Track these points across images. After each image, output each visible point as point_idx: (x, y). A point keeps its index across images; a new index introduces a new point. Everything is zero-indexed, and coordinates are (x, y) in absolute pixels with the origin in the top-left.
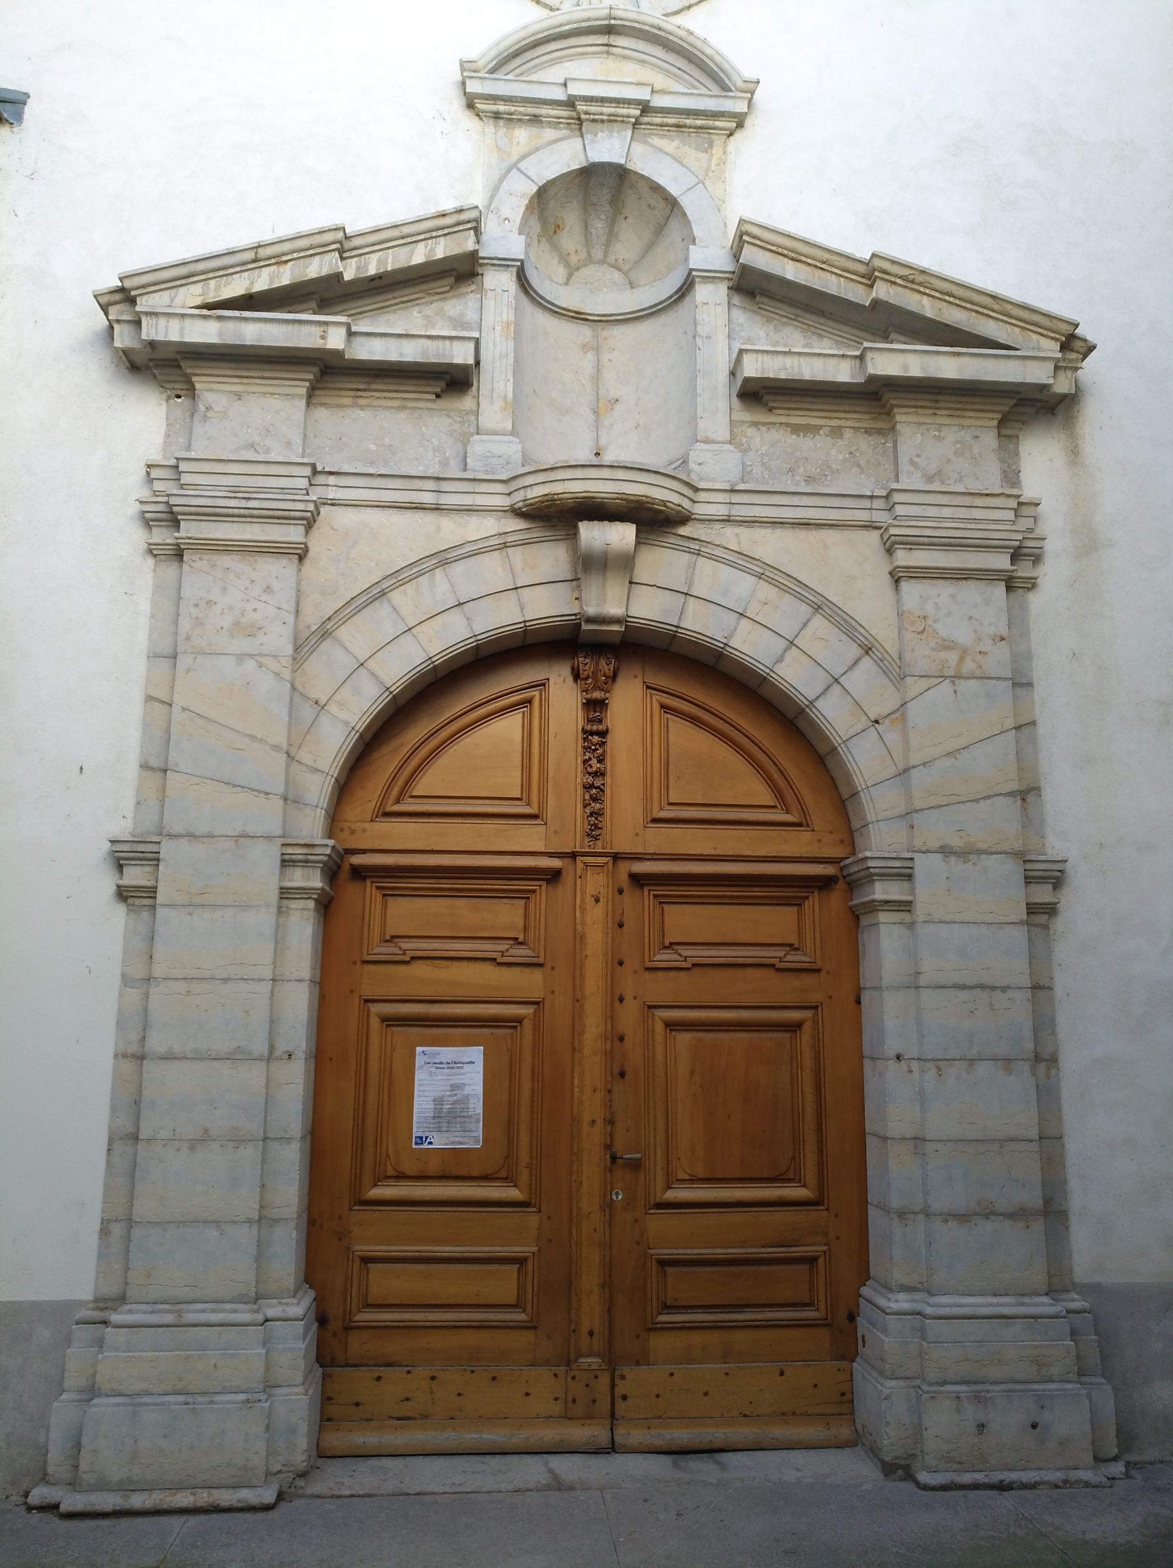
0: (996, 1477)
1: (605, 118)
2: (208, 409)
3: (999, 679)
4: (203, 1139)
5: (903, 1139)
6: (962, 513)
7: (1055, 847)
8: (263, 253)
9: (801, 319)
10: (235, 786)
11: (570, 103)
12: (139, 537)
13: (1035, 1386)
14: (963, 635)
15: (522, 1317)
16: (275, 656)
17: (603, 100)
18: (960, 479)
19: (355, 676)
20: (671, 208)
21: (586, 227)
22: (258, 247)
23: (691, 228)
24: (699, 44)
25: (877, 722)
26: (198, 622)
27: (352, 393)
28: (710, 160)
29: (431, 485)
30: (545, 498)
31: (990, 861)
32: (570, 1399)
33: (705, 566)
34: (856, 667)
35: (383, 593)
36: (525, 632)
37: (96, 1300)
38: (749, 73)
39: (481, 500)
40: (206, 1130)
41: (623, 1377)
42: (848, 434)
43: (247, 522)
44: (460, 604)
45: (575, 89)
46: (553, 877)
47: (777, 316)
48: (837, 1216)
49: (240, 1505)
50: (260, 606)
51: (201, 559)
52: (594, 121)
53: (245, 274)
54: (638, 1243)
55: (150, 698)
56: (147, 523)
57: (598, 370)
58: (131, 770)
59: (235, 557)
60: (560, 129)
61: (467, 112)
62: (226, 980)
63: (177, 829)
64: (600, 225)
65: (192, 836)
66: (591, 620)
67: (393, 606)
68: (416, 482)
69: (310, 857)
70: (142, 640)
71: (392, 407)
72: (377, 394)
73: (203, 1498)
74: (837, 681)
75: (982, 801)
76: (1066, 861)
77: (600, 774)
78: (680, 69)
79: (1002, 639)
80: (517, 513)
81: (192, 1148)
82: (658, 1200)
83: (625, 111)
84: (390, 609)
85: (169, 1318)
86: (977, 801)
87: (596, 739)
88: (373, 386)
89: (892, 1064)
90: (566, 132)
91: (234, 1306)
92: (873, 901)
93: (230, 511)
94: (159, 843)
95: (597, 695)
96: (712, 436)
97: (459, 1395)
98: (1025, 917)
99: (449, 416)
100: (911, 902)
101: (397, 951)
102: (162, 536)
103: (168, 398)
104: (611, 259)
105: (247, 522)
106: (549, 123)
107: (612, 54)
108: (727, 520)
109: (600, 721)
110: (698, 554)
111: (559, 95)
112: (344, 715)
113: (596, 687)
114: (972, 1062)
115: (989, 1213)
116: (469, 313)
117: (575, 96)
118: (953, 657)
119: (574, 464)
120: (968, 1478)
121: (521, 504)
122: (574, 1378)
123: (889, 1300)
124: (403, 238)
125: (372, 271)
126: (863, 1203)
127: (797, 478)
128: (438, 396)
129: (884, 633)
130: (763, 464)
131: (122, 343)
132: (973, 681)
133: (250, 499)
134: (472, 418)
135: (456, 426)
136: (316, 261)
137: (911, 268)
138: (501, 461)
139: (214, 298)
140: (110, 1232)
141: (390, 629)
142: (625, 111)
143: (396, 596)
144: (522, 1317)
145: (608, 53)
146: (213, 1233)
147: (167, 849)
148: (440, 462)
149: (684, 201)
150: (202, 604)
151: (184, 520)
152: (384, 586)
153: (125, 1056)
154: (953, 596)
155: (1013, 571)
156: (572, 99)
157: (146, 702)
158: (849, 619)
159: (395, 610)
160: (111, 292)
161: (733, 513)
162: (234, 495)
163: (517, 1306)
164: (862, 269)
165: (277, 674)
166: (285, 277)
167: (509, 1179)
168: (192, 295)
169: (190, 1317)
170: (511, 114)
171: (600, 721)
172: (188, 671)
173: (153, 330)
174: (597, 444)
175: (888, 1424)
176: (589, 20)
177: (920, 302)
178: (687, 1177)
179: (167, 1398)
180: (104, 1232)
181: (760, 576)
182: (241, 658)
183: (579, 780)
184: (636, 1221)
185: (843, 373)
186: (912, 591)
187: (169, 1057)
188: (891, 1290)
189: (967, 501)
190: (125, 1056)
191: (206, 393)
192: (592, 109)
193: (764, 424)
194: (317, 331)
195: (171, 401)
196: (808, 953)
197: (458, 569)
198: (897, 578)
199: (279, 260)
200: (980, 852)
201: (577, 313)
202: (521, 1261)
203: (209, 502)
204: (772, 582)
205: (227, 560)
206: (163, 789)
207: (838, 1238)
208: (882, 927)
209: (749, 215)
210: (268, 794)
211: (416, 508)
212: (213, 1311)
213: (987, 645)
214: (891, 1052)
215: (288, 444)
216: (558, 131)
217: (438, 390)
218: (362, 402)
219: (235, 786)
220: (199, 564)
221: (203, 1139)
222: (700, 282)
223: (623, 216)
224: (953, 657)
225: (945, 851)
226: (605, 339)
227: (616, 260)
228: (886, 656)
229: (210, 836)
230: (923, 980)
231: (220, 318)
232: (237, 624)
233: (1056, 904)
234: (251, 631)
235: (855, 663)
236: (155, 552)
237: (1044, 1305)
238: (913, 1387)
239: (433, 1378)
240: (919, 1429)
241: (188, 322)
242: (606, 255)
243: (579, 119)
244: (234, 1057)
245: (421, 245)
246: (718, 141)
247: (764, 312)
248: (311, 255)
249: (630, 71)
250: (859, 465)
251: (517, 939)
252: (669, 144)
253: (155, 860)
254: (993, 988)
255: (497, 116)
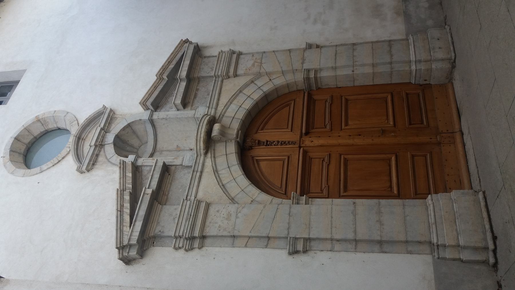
0: (451, 44)
1: (102, 138)
2: (160, 231)
3: (262, 56)
4: (380, 222)
5: (373, 69)
6: (222, 62)
7: (304, 46)
8: (119, 209)
9: (167, 97)
10: (275, 217)
11: (96, 146)
12: (196, 252)
13: (429, 40)
14: (252, 62)
15: (428, 155)
16: (238, 208)
17: (98, 138)
18: (214, 65)
19: (245, 192)
20: (130, 127)
21: (127, 151)
22: (117, 210)
23: (137, 120)
24: (90, 117)
25: (270, 80)
26: (225, 230)
27: (164, 196)
28: (120, 117)
29: (195, 173)
30: (204, 143)
31: (305, 55)
32: (449, 142)
33: (227, 114)
34: (256, 84)
35: (223, 185)
36: (238, 153)
37: (432, 254)
38: (101, 106)
39: (201, 162)
40: (377, 221)
41: (442, 131)
42: (198, 87)
43: (197, 217)
44: (229, 167)
45: (93, 143)
46: (305, 153)
47: (165, 102)
48: (395, 89)
49: (484, 200)
50: (222, 213)
51: (206, 230)
52: (102, 141)
53: (124, 215)
54: (405, 130)
55: (246, 246)
56: (192, 249)
57: (168, 151)
58: (267, 251)
59: (207, 220)
60: (101, 150)
61: (90, 172)
62: (332, 217)
63: (286, 232)
64: (128, 148)
65: (288, 229)
66: (237, 137)
67: (227, 183)
68: (193, 177)
69: (297, 198)
70: (228, 250)
71: (170, 186)
72: (165, 189)
73: (484, 210)
74: (259, 88)
75: (291, 57)
76: (306, 42)
77: (278, 142)
78: (94, 124)
79: (253, 55)
80: (206, 153)
81: (383, 225)
82: (393, 126)
83: (102, 134)
84: (228, 184)
85: (434, 226)
86: (291, 58)
87: (268, 143)
88: (163, 189)
89: (355, 72)
90: (102, 149)
91: (429, 211)
92: (314, 77)
93: (193, 221)
94: (290, 237)
95: (257, 142)
96: (194, 114)
97: (452, 168)
98: (319, 48)
99: (176, 172)
100: (315, 70)
101: (325, 189)
102: (196, 244)
103: (153, 246)
104: (138, 147)
105: (197, 217)
106: (99, 152)
107: (85, 139)
108: (216, 109)
109: (264, 142)
110: (224, 115)
111: (93, 148)
112: (256, 195)
113: (255, 142)
114: (353, 56)
115: (390, 51)
116: (147, 169)
117: (95, 144)
118: (256, 64)
119: (196, 134)
120: (452, 48)
121: (204, 151)
122: (443, 141)
123: (413, 70)
124: (123, 178)
125: (131, 186)
126: (391, 84)
127: (207, 97)
128: (169, 175)
129: (248, 78)
130: (203, 104)
131: (135, 252)
132: (263, 60)
133: (191, 215)
134: (177, 167)
135: (179, 170)
136: (125, 197)
137: (161, 68)
138: (191, 157)
139: (128, 224)
140: (411, 251)
141: (234, 184)
142: (102, 134)
143: (224, 182)
144: (428, 155)
145: (84, 140)
146: (408, 218)
147: (292, 235)
148: (188, 174)
149: (129, 122)
150: (219, 229)
151: (193, 234)
152: (221, 185)
153: (356, 249)
154: (242, 64)
155: (237, 54)
156: (95, 144)
157: (247, 247)
158: (244, 85)
159: (228, 183)
160: (119, 253)
161: (214, 107)
162: (189, 219)
163: (425, 156)
164: (158, 80)
165: (243, 208)
166: (127, 205)
167: (390, 160)
168: (127, 229)
169: (433, 221)
170: (94, 160)
171: (264, 142)
172: (239, 232)
173: (134, 241)
174: (188, 150)
175: (442, 67)
176: (75, 141)
177: (169, 68)
178: (387, 121)
179: (457, 225)
180: (410, 253)
181: (231, 103)
182: (237, 217)
183: (279, 147)
184: (399, 130)
185: (184, 84)
186: (240, 72)
187: (355, 232)
188: (411, 70)
189: (219, 62)
190: (356, 249)
191: (155, 232)
192: (99, 141)
193: (192, 104)
194: (146, 196)
195: (155, 245)
196: (327, 98)
197: (219, 168)
198: (236, 75)
199: (122, 206)
200: (303, 57)
201: (151, 155)
202: (413, 156)
203: (189, 226)
204: (233, 101)
205: (207, 223)
206: (275, 238)
207: (401, 89)
208: (321, 76)
209: (139, 101)
210: (277, 209)
211: (200, 177)
212: (431, 216)
213: (254, 58)
214: (352, 73)
215: (176, 209)
216: (102, 151)
217: (168, 174)
218: (167, 193)
219: (275, 217)
220: (207, 231)
221: (380, 222)
222: (152, 118)
223: (128, 142)
224: (256, 64)
225: (303, 63)
226: (159, 149)
227: (138, 146)
228: (255, 78)
229: (289, 223)
230: (334, 65)
231: (135, 221)
232: (227, 219)
233: (316, 45)
234: (229, 215)
235: (256, 84)
236: (201, 246)
237: (411, 41)
238: (433, 62)
239: (448, 175)
240: (443, 60)
241: (134, 230)
242: (136, 149)
243: (100, 145)
244: (355, 214)
245: (127, 174)
246: (116, 116)
247: (163, 105)
248: (123, 198)
249: (90, 136)
250: (206, 85)
251: (322, 160)
252: (113, 126)
253: (296, 239)
254: (336, 53)
255: (93, 164)
